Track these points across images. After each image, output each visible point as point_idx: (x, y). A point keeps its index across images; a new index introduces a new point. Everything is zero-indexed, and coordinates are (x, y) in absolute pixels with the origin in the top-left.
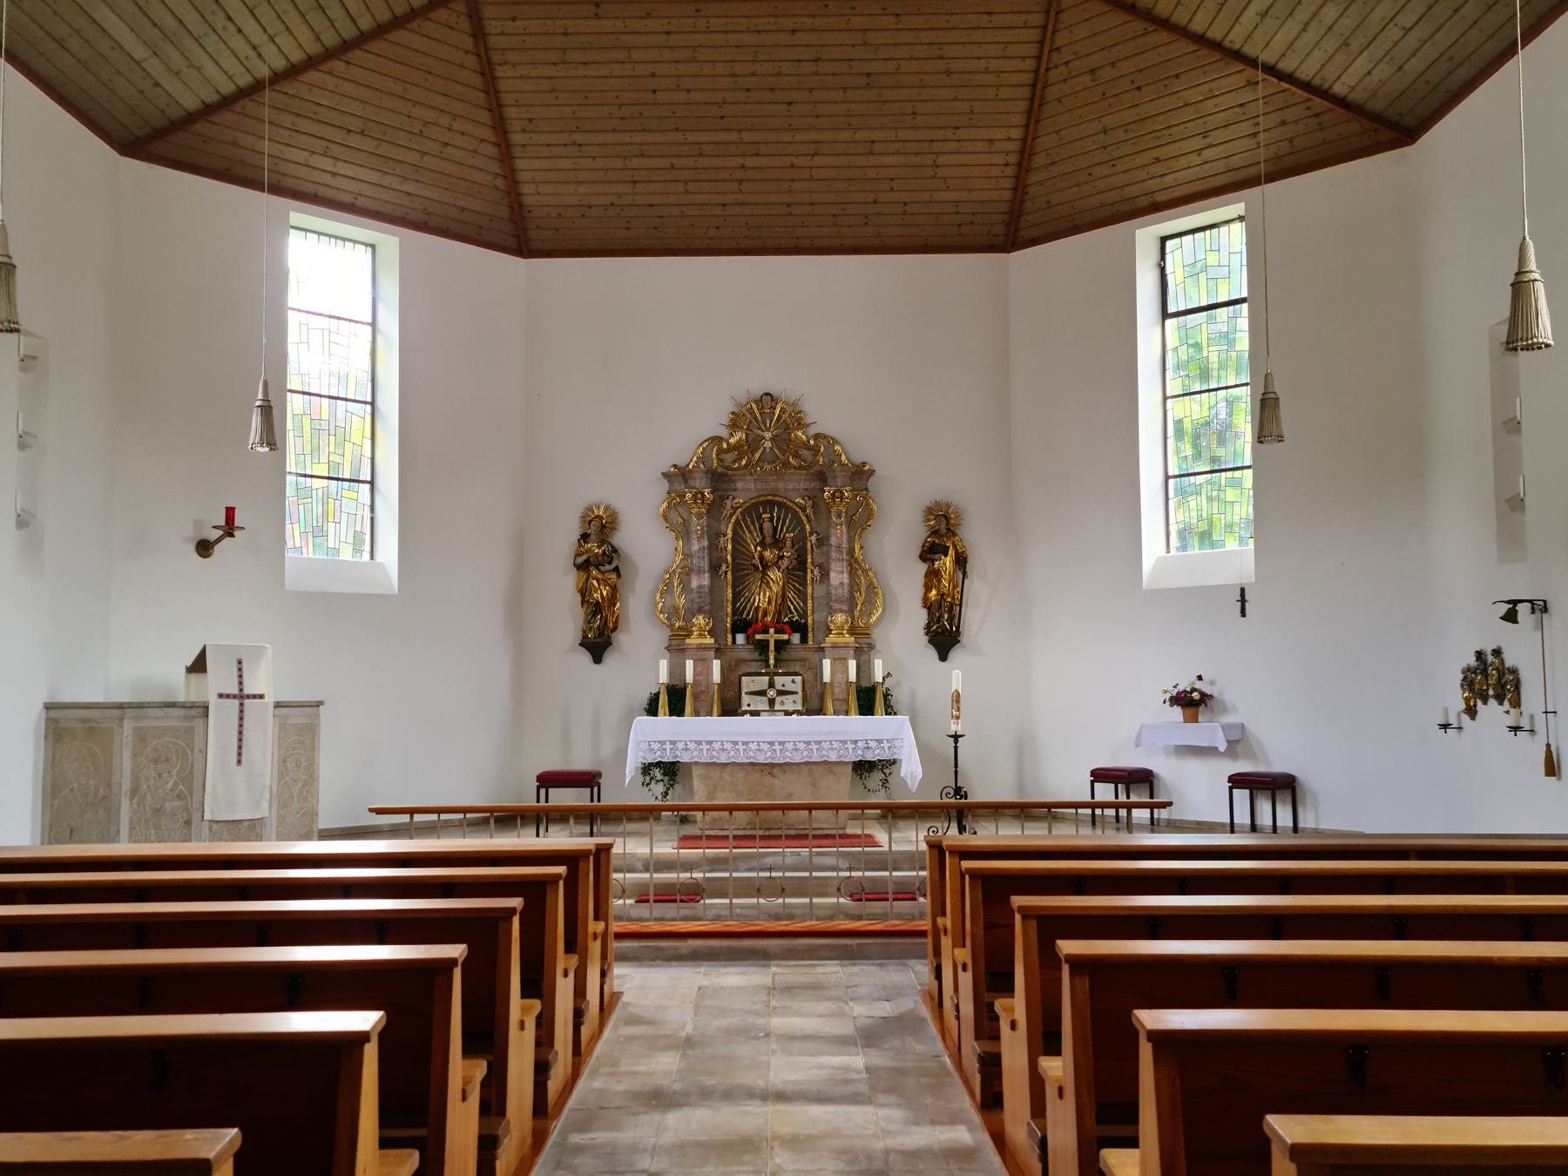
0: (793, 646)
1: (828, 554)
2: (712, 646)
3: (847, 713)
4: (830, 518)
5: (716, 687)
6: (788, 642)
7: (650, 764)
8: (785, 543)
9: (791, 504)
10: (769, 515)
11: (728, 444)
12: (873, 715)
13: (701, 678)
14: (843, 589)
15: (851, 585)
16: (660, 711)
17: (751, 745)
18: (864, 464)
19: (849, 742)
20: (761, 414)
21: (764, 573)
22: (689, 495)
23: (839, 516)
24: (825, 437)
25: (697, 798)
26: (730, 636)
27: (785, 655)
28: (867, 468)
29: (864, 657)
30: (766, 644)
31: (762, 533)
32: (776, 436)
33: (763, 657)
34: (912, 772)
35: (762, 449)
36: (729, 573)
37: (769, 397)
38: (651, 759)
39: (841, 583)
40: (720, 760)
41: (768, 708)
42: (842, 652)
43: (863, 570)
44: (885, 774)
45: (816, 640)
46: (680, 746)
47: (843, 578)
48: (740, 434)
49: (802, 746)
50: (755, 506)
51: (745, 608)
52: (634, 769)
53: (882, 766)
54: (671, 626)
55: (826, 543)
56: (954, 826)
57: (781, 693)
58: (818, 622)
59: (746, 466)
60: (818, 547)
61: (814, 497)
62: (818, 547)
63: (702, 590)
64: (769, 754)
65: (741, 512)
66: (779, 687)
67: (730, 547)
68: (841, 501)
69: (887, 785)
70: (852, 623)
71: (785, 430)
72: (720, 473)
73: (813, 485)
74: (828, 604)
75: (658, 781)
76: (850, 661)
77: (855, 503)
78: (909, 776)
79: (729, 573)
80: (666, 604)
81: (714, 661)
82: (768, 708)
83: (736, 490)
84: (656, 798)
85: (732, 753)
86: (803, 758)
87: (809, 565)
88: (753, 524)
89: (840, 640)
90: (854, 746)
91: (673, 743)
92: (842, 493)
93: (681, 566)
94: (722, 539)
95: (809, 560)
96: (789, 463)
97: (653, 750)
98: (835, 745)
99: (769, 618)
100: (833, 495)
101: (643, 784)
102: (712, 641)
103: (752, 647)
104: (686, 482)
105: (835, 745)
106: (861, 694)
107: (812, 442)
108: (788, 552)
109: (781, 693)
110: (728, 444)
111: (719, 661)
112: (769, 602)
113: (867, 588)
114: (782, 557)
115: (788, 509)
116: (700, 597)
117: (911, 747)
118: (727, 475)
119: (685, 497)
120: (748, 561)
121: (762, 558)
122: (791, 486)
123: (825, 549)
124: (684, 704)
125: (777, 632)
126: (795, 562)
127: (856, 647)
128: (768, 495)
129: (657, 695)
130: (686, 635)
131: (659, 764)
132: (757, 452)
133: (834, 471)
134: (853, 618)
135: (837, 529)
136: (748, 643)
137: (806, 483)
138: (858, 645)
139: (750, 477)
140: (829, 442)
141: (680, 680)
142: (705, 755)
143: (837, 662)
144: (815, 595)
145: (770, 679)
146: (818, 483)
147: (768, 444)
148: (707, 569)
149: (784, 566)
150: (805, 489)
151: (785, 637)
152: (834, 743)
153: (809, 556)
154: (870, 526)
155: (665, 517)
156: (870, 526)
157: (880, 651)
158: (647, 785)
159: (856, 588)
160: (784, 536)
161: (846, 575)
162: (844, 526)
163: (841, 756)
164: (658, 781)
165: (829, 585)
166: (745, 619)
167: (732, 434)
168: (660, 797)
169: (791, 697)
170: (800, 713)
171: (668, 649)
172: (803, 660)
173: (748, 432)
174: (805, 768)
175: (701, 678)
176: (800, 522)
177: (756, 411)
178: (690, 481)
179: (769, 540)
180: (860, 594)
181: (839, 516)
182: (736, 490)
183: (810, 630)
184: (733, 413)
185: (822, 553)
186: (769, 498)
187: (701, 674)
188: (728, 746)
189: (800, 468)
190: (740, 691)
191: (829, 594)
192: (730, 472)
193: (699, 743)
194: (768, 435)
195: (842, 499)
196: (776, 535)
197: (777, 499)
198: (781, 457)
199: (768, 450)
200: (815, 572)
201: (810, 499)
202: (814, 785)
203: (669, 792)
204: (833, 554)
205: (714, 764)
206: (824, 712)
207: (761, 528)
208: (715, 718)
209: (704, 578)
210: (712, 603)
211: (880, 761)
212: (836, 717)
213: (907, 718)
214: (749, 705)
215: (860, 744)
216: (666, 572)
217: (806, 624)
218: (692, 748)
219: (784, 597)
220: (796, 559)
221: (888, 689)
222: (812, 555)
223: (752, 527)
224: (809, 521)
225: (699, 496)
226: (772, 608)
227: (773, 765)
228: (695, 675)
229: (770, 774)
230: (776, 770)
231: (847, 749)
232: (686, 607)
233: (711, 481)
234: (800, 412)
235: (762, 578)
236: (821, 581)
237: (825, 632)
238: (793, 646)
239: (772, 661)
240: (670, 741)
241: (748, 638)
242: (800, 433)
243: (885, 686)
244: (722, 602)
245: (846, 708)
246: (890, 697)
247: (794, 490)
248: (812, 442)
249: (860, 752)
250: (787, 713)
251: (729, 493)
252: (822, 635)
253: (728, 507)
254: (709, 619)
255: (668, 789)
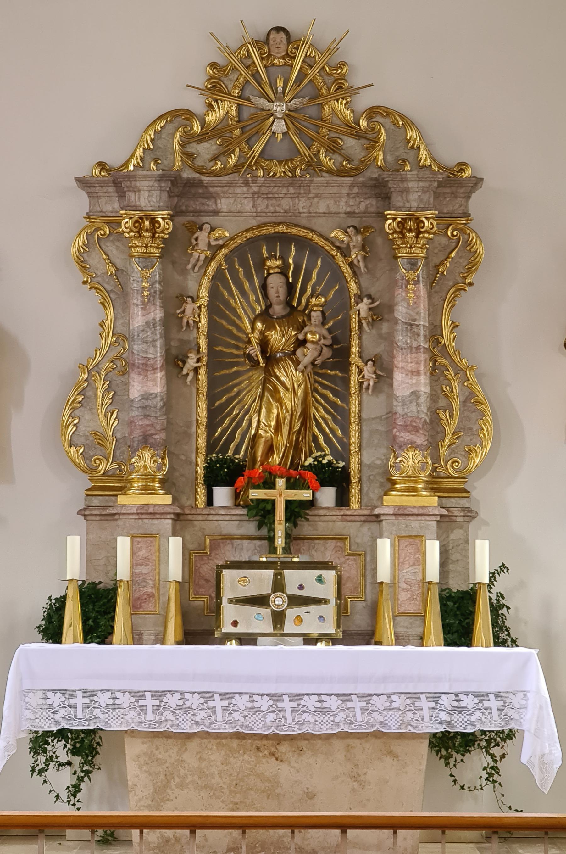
0: (322, 512)
1: (390, 339)
2: (169, 510)
3: (421, 641)
4: (394, 269)
5: (173, 590)
6: (311, 504)
7: (47, 734)
8: (309, 317)
9: (321, 242)
10: (279, 263)
11: (203, 124)
12: (469, 644)
13: (144, 570)
14: (418, 405)
15: (433, 397)
16: (67, 633)
17: (306, 701)
18: (462, 166)
19: (423, 697)
20: (266, 67)
21: (269, 372)
22: (127, 223)
23: (413, 266)
24: (388, 113)
25: (133, 800)
26: (202, 491)
27: (305, 528)
28: (468, 173)
29: (456, 535)
30: (269, 507)
31: (266, 295)
32: (296, 110)
33: (264, 532)
34: (543, 755)
35: (268, 134)
36: (202, 371)
37: (282, 35)
38: (44, 726)
39: (414, 393)
40: (177, 726)
41: (271, 630)
42: (415, 525)
43: (458, 370)
44: (493, 756)
45: (365, 500)
46: (103, 699)
47: (418, 384)
48: (226, 105)
49: (333, 703)
50: (253, 243)
51: (231, 438)
52: (13, 742)
53: (488, 742)
54: (91, 470)
55: (386, 316)
56: (99, 838)
57: (295, 601)
58: (369, 466)
59: (237, 168)
60: (373, 323)
61: (367, 228)
62: (373, 323)
63: (149, 403)
64: (271, 717)
65: (226, 256)
66: (292, 589)
67: (204, 321)
68: (417, 237)
69: (496, 777)
70: (435, 469)
71: (313, 99)
72: (188, 180)
73: (362, 207)
74: (389, 432)
75: (61, 765)
76: (428, 542)
77: (444, 241)
78: (536, 762)
79: (202, 371)
80: (82, 428)
81: (171, 539)
82: (271, 630)
83: (216, 213)
84: (58, 797)
85: (202, 715)
86: (336, 725)
87: (354, 358)
88: (249, 278)
89: (409, 501)
90: (433, 704)
91: (89, 693)
92: (418, 221)
93: (113, 354)
94: (189, 307)
95: (355, 349)
96: (320, 161)
97: (51, 707)
98: (398, 702)
99: (276, 459)
100: (402, 224)
101: (33, 770)
102: (167, 500)
103: (245, 511)
104: (122, 195)
105: (398, 702)
106: (450, 604)
107: (363, 123)
108: (313, 333)
109: (295, 601)
110: (203, 124)
111: (180, 539)
112: (278, 428)
113: (464, 403)
114: (302, 343)
115: (316, 250)
116: (147, 416)
117: (541, 707)
118: (200, 183)
119: (119, 224)
120: (237, 348)
121: (264, 344)
122: (322, 208)
123: (385, 327)
124: (113, 619)
125: (290, 485)
126: (327, 353)
127: (442, 516)
128: (279, 224)
129: (62, 601)
130: (120, 489)
131: (62, 734)
132: (258, 140)
133: (403, 180)
134: (436, 459)
135: (407, 292)
136: (237, 505)
137: (351, 203)
138: (444, 512)
139: (245, 189)
140: (395, 124)
141: (107, 573)
142: (80, 715)
143: (404, 543)
144: (364, 416)
145: (276, 575)
146: (374, 202)
147: (280, 126)
148: (159, 364)
149: (306, 360)
150: (350, 214)
151: (306, 495)
152: (394, 697)
153: (355, 342)
154: (471, 284)
155: (83, 265)
156: (471, 284)
157: (486, 523)
158: (40, 772)
159: (442, 402)
160: (308, 301)
161: (424, 379)
162: (421, 285)
163: (408, 723)
164: (61, 765)
165: (391, 396)
166: (232, 460)
167: (210, 106)
168: (64, 795)
169: (314, 609)
170: (333, 640)
171: (83, 513)
172: (341, 538)
173: (241, 102)
174: (338, 744)
175: (144, 570)
176: (338, 276)
177: (256, 59)
178: (131, 196)
179: (278, 310)
180: (451, 416)
181: (413, 266)
182: (216, 213)
183: (354, 480)
184: (213, 65)
185: (380, 336)
186: (281, 229)
187: (146, 561)
188: (194, 701)
189: (340, 172)
190: (219, 596)
191: (391, 415)
192: (205, 179)
193: (138, 694)
194: (279, 108)
195: (418, 233)
196: (292, 299)
197: (294, 231)
198: (303, 149)
199: (279, 137)
200: (365, 373)
201: (357, 231)
202: (355, 778)
203: (83, 786)
204: (401, 338)
205: (167, 735)
206: (377, 638)
207: (264, 287)
208: (170, 648)
209: (154, 380)
210: (168, 427)
211: (484, 732)
212: (399, 648)
213: (534, 652)
214: (235, 623)
215: (445, 701)
216: (83, 367)
217: (346, 472)
218: (334, 708)
219: (305, 415)
220: (330, 346)
221: (501, 596)
222: (360, 338)
223: (247, 285)
224: (355, 274)
225: (147, 223)
226: (283, 440)
227: (278, 739)
228: (134, 564)
229: (272, 754)
230: (284, 748)
231: (420, 709)
232: (119, 435)
233: (170, 195)
234: (342, 64)
235: (265, 381)
236: (377, 389)
237: (382, 485)
238: (322, 512)
239: (280, 541)
240: (84, 691)
241: (236, 496)
242: (340, 106)
243: (494, 590)
244: (189, 425)
245: (420, 630)
246: (504, 611)
247: (328, 214)
248: (363, 123)
249: (443, 716)
250: (309, 640)
251: (205, 219)
252: (378, 491)
253: (202, 245)
254: (163, 459)
255: (80, 780)
